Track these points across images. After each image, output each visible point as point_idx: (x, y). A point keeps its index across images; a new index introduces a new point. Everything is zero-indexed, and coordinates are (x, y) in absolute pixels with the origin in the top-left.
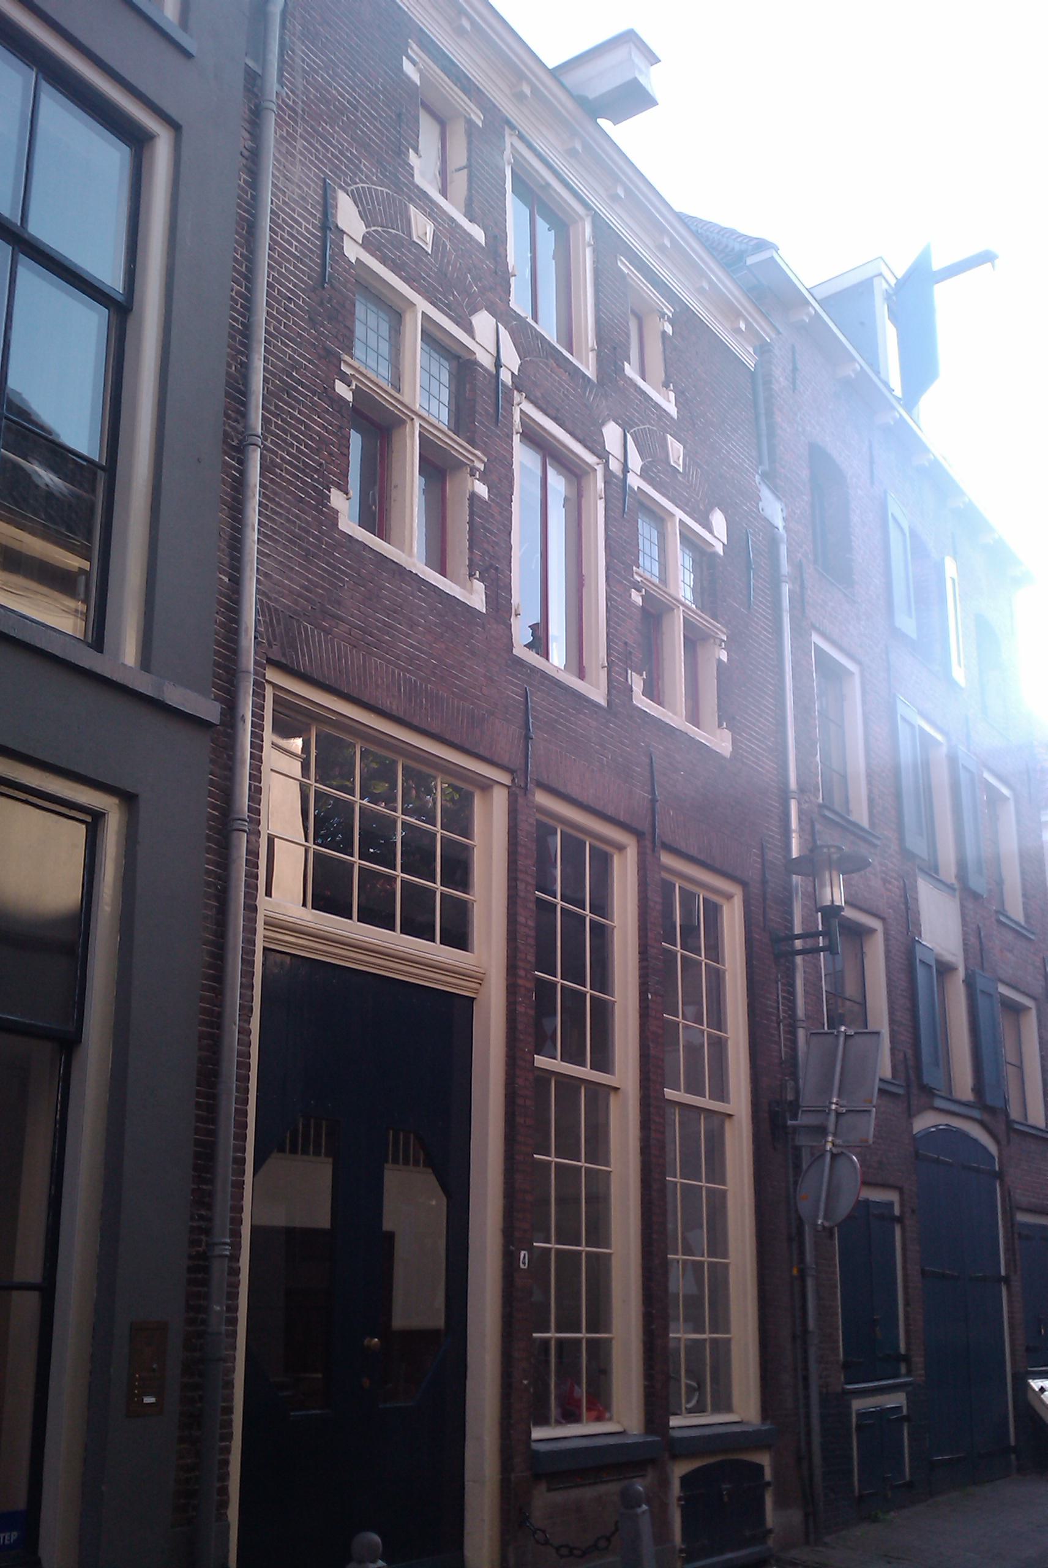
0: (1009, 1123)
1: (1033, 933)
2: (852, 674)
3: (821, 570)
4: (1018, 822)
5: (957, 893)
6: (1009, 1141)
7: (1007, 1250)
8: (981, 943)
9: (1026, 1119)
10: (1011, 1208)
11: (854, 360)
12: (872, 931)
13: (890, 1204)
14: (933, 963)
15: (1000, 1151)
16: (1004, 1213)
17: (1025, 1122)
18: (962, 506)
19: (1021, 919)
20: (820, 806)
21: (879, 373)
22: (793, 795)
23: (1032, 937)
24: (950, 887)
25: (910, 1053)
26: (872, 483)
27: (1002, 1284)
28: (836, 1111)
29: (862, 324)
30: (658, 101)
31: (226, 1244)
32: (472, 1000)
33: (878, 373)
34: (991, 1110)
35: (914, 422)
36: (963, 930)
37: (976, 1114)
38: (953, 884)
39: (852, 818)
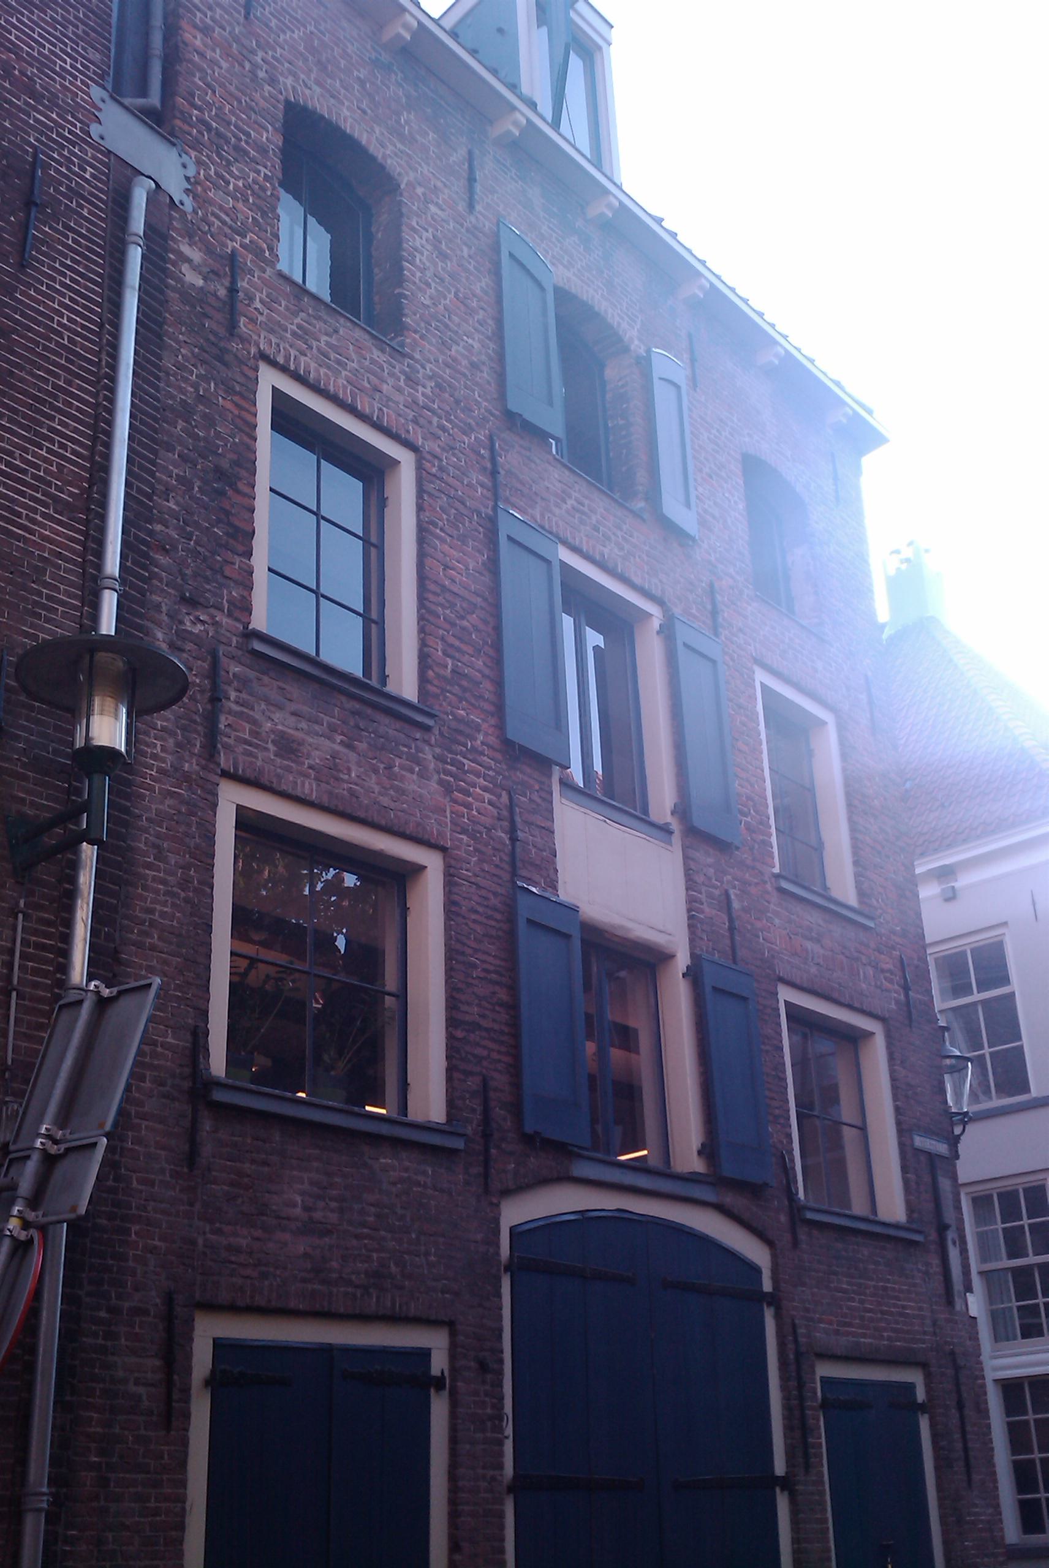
0: (795, 1210)
1: (871, 918)
2: (824, 723)
3: (363, 325)
4: (844, 756)
5: (676, 839)
6: (795, 1243)
7: (788, 1428)
8: (731, 920)
9: (874, 1210)
10: (798, 1355)
11: (514, 108)
12: (418, 869)
13: (424, 1355)
14: (576, 934)
15: (774, 1258)
16: (783, 1364)
17: (872, 1217)
18: (844, 421)
19: (852, 900)
20: (777, 876)
21: (536, 105)
22: (108, 582)
23: (871, 924)
24: (665, 830)
25: (500, 1080)
26: (471, 206)
27: (778, 1490)
28: (44, 1150)
29: (500, 31)
30: (880, 421)
31: (44, 1494)
32: (982, 1263)
33: (513, 87)
34: (754, 1190)
35: (606, 176)
36: (687, 895)
37: (708, 1195)
38: (667, 824)
39: (390, 688)
